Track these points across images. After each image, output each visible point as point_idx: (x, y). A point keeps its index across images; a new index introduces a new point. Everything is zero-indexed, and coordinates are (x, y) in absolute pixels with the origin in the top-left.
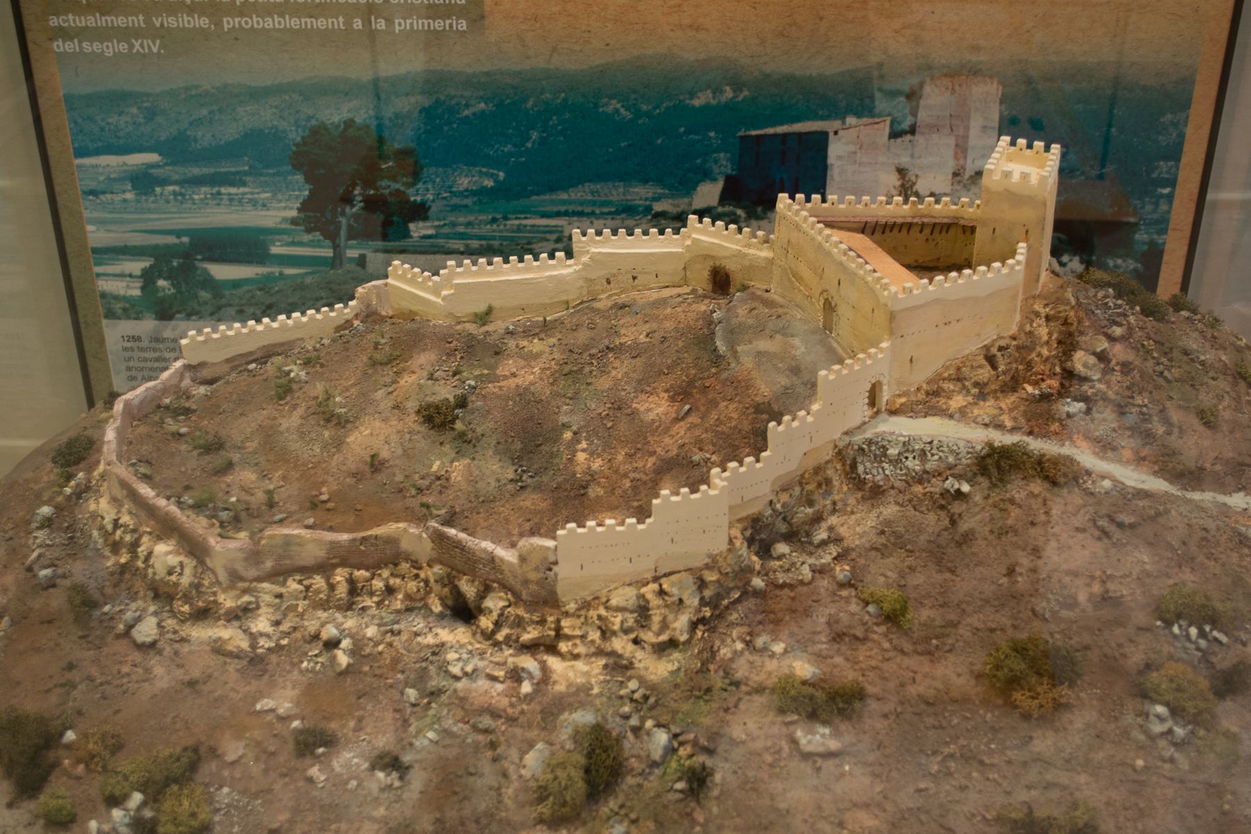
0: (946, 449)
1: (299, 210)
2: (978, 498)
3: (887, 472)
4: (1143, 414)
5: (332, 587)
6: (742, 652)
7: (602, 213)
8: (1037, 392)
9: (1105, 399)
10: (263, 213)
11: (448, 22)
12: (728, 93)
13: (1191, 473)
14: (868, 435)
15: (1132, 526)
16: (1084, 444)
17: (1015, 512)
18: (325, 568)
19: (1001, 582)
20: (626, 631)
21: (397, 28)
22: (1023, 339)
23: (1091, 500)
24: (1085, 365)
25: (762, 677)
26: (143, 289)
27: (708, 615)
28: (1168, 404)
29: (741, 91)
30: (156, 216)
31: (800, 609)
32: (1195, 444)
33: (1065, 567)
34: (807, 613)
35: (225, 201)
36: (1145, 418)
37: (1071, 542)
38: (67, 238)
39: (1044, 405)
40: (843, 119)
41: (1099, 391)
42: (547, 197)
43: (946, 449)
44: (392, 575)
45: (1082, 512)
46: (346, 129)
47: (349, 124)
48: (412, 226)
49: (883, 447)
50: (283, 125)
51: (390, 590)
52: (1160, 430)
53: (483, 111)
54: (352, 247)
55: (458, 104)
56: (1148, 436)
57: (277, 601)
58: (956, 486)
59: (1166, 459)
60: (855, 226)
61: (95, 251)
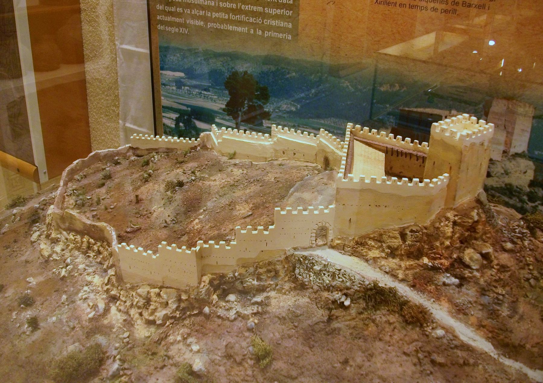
0: (348, 277)
1: (226, 105)
2: (353, 312)
3: (311, 278)
4: (498, 299)
5: (82, 242)
6: (179, 342)
7: (337, 133)
8: (430, 264)
9: (477, 283)
10: (214, 104)
11: (284, 35)
12: (397, 87)
13: (514, 347)
14: (305, 253)
15: (441, 365)
16: (446, 305)
17: (372, 328)
18: (82, 233)
19: (336, 365)
20: (139, 308)
21: (266, 35)
22: (431, 231)
23: (424, 339)
24: (471, 259)
25: (181, 359)
26: (176, 125)
27: (178, 316)
28: (522, 299)
31: (219, 333)
32: (520, 331)
33: (380, 373)
34: (220, 337)
35: (203, 97)
36: (498, 302)
37: (395, 359)
38: (155, 100)
39: (432, 273)
40: (450, 111)
41: (475, 277)
42: (316, 120)
43: (348, 277)
44: (101, 246)
45: (414, 344)
46: (244, 75)
47: (246, 73)
48: (264, 121)
49: (313, 263)
50: (224, 69)
51: (99, 252)
52: (505, 312)
53: (294, 77)
54: (242, 125)
55: (285, 71)
56: (493, 314)
57: (65, 241)
58: (342, 300)
59: (500, 332)
60: (383, 148)
61: (163, 107)
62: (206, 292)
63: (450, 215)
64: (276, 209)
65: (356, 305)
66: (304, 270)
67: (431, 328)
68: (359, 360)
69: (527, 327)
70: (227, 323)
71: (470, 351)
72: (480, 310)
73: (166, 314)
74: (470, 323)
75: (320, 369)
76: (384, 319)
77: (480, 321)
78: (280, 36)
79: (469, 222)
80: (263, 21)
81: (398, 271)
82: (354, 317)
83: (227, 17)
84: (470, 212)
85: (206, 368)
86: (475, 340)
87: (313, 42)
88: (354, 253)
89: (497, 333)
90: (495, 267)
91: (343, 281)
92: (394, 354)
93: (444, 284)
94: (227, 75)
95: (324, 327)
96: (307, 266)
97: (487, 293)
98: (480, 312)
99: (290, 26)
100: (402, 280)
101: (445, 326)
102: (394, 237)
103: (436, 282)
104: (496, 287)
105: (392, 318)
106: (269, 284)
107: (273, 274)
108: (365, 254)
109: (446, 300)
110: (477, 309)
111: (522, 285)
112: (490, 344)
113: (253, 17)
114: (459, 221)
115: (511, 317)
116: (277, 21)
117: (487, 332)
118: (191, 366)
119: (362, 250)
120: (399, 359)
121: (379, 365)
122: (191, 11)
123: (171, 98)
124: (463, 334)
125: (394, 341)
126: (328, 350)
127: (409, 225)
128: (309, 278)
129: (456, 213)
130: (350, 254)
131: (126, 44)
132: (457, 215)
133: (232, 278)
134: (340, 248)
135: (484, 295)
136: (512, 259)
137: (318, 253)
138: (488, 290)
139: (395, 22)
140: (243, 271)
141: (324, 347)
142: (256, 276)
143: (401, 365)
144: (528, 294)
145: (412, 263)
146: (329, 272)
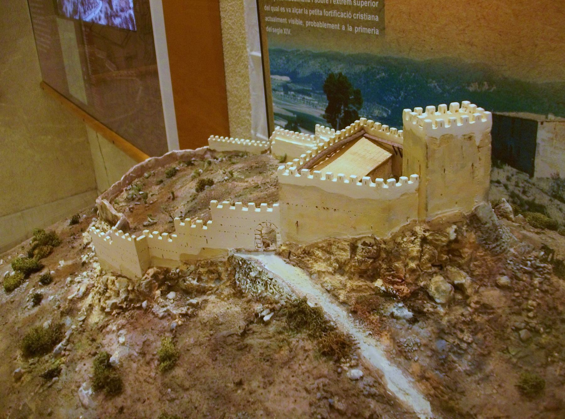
1: (326, 111)
8: (383, 288)
12: (486, 87)
16: (386, 341)
17: (285, 352)
19: (229, 385)
23: (335, 376)
24: (437, 289)
28: (497, 354)
29: (493, 86)
30: (288, 104)
33: (268, 404)
36: (460, 352)
37: (291, 393)
41: (437, 313)
45: (321, 380)
46: (339, 78)
47: (340, 74)
49: (250, 268)
50: (322, 72)
55: (375, 71)
56: (444, 364)
61: (275, 114)
62: (146, 285)
63: (419, 229)
64: (212, 201)
65: (277, 322)
66: (243, 276)
67: (348, 365)
68: (254, 384)
69: (489, 391)
70: (156, 320)
71: (392, 406)
72: (428, 356)
73: (116, 303)
74: (410, 371)
75: (212, 385)
76: (301, 343)
77: (424, 370)
78: (369, 31)
79: (442, 242)
80: (352, 15)
81: (340, 291)
82: (271, 335)
83: (321, 14)
84: (446, 228)
85: (120, 361)
86: (407, 394)
87: (399, 35)
88: (300, 264)
89: (442, 392)
90: (473, 305)
91: (273, 292)
92: (293, 386)
93: (392, 315)
94: (325, 77)
95: (236, 341)
96: (245, 271)
97: (446, 337)
98: (428, 360)
99: (377, 19)
100: (343, 303)
101: (370, 368)
102: (342, 249)
103: (382, 311)
104: (462, 331)
105: (309, 345)
106: (211, 287)
107: (215, 276)
108: (310, 266)
109: (389, 336)
110: (425, 354)
111: (506, 335)
112: (428, 403)
113: (343, 12)
114: (430, 238)
115: (469, 374)
116: (365, 15)
117: (430, 387)
118: (109, 356)
119: (308, 261)
120: (297, 394)
121: (272, 395)
122: (292, 10)
123: (280, 104)
124: (393, 382)
125: (300, 371)
126: (230, 366)
127: (361, 236)
128: (245, 285)
129: (428, 228)
130: (294, 263)
131: (255, 51)
132: (428, 230)
133: (175, 274)
134: (286, 255)
135: (442, 339)
136: (504, 299)
137: (261, 258)
138: (448, 334)
139: (480, 4)
140: (184, 268)
141: (227, 363)
142: (197, 275)
143: (296, 401)
144: (510, 349)
145: (361, 284)
146: (262, 280)
